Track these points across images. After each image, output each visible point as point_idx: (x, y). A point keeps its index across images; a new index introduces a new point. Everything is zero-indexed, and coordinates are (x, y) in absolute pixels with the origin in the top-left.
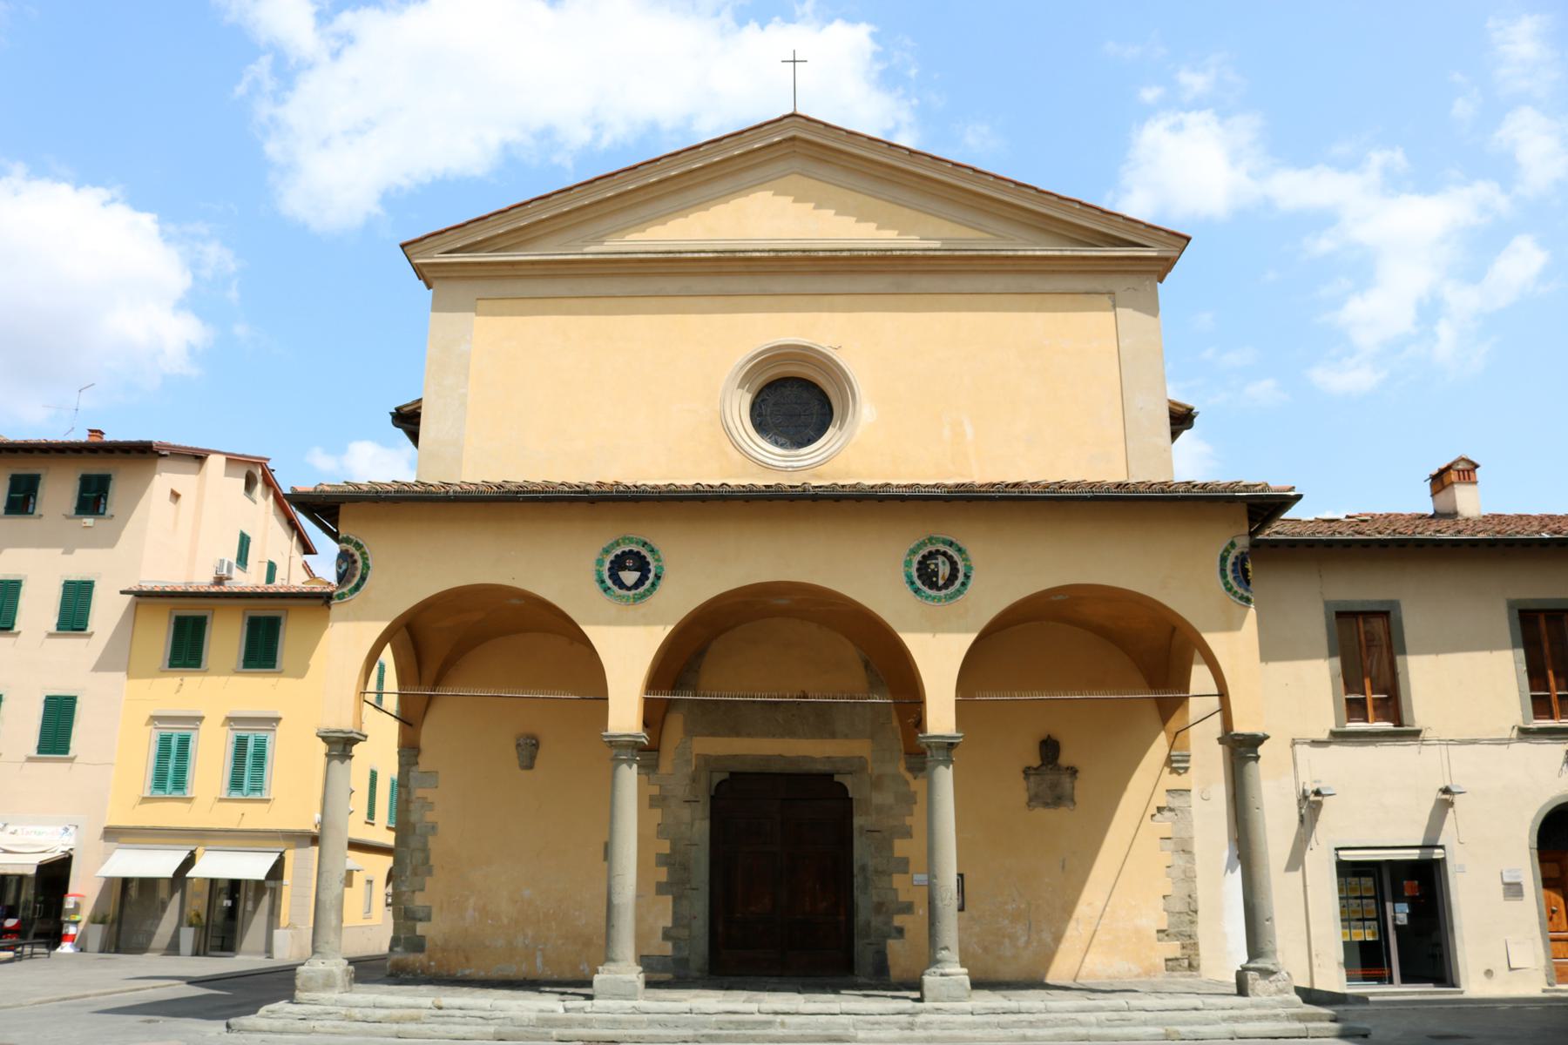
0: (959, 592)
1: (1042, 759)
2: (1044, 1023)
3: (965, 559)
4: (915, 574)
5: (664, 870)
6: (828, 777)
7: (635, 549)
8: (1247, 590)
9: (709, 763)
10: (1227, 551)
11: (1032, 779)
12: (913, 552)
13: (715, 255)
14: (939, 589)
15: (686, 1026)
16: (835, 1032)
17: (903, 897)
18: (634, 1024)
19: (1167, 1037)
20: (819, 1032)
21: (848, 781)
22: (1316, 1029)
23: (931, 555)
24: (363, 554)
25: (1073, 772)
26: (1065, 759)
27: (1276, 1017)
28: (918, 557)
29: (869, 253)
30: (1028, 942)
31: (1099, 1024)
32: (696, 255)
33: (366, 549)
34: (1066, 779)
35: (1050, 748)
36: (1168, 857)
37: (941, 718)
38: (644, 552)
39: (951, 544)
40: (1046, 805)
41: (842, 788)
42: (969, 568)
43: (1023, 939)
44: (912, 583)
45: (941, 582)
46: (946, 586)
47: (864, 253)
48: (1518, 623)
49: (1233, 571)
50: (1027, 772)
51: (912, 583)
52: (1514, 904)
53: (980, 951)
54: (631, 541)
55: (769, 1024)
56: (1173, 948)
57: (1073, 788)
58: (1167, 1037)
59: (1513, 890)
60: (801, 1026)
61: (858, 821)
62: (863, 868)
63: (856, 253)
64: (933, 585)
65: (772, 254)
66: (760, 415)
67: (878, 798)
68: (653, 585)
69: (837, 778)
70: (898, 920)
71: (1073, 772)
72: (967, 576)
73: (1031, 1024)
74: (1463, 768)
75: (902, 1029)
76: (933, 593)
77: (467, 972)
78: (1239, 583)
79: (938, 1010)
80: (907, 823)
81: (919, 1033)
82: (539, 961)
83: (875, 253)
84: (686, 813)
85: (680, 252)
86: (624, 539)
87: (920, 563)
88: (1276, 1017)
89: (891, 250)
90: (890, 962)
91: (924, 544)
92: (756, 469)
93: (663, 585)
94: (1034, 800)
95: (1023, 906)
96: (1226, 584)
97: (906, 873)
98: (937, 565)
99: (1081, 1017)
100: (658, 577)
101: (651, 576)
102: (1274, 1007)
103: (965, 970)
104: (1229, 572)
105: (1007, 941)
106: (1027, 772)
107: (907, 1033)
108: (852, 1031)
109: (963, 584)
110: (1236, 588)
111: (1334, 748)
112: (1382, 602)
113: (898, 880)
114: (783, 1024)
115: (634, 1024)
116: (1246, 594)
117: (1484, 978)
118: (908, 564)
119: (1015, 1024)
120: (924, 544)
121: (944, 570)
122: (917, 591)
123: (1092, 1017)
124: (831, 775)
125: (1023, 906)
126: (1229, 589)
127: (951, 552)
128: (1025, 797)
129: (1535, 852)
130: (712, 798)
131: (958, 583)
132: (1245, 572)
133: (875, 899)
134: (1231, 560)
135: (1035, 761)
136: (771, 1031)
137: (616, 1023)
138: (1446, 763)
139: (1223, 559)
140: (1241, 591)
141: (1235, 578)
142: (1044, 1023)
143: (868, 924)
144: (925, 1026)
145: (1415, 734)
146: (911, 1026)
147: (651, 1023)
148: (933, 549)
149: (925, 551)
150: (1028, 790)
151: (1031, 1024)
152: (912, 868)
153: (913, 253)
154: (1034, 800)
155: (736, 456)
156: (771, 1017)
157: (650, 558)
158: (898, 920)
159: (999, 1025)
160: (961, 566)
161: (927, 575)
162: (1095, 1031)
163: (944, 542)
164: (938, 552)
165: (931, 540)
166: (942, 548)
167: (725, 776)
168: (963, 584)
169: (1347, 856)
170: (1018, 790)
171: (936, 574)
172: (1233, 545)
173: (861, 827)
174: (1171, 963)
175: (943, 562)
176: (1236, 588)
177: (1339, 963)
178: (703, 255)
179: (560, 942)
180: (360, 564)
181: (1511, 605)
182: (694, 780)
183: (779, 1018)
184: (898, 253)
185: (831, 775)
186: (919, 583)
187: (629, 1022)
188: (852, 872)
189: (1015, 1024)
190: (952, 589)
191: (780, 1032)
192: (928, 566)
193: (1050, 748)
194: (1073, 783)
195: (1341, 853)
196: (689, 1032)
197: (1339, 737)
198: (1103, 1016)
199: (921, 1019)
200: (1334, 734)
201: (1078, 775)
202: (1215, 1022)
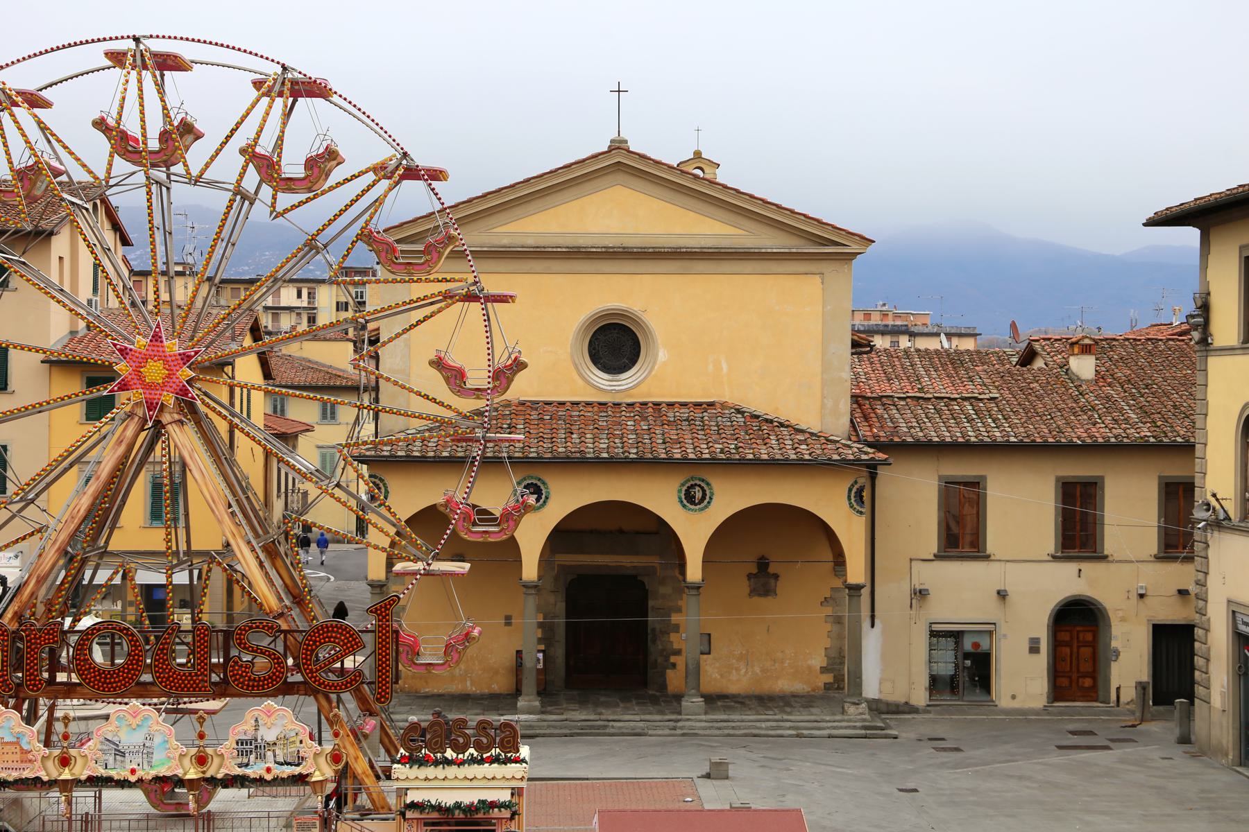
0: (706, 507)
1: (758, 569)
2: (739, 728)
3: (711, 489)
4: (683, 497)
5: (540, 630)
6: (635, 577)
7: (534, 482)
8: (861, 507)
9: (564, 569)
10: (853, 485)
11: (752, 580)
12: (683, 485)
13: (567, 250)
14: (696, 505)
15: (565, 728)
16: (638, 731)
17: (676, 646)
18: (540, 728)
19: (798, 736)
20: (630, 731)
21: (646, 580)
22: (871, 734)
23: (693, 486)
24: (384, 484)
25: (776, 577)
26: (772, 569)
27: (855, 728)
28: (685, 488)
29: (666, 250)
30: (746, 672)
31: (767, 728)
32: (555, 250)
33: (386, 481)
34: (772, 581)
35: (763, 565)
36: (829, 627)
37: (694, 571)
38: (539, 483)
39: (703, 480)
40: (760, 595)
41: (643, 583)
42: (712, 494)
43: (744, 671)
44: (682, 502)
45: (697, 501)
46: (700, 503)
47: (663, 250)
48: (1060, 491)
49: (855, 497)
50: (750, 576)
51: (682, 502)
52: (1034, 656)
53: (719, 677)
54: (532, 478)
55: (605, 727)
56: (828, 678)
57: (776, 586)
58: (798, 736)
59: (1034, 649)
60: (620, 728)
61: (651, 603)
62: (654, 630)
63: (657, 250)
64: (693, 503)
65: (603, 250)
66: (594, 349)
67: (664, 590)
68: (544, 502)
69: (639, 578)
70: (673, 659)
71: (776, 577)
72: (711, 498)
73: (733, 728)
74: (1016, 578)
75: (670, 729)
76: (692, 507)
77: (427, 690)
78: (857, 504)
79: (688, 720)
80: (679, 604)
81: (679, 732)
82: (468, 684)
83: (670, 250)
84: (552, 599)
85: (544, 247)
86: (528, 477)
87: (686, 490)
88: (855, 728)
89: (681, 248)
90: (668, 682)
91: (688, 480)
92: (593, 391)
93: (551, 503)
94: (754, 592)
95: (744, 652)
96: (850, 503)
97: (678, 632)
98: (695, 493)
99: (758, 724)
100: (547, 498)
101: (543, 497)
102: (855, 722)
103: (702, 699)
104: (852, 497)
105: (734, 671)
106: (750, 576)
107: (673, 732)
108: (646, 731)
109: (709, 503)
110: (855, 506)
111: (935, 563)
112: (975, 476)
113: (673, 637)
114: (613, 727)
115: (540, 728)
116: (860, 510)
117: (1011, 700)
118: (680, 491)
119: (726, 728)
120: (688, 480)
121: (699, 495)
122: (684, 506)
123: (763, 725)
124: (636, 576)
125: (744, 652)
126: (851, 507)
127: (703, 484)
128: (748, 590)
129: (1050, 628)
130: (567, 589)
131: (706, 502)
132: (861, 497)
133: (660, 647)
134: (854, 490)
135: (755, 571)
136: (607, 731)
137: (531, 727)
138: (1003, 574)
139: (850, 490)
140: (858, 508)
141: (855, 501)
142: (739, 728)
143: (656, 661)
144: (681, 728)
145: (988, 556)
146: (674, 728)
147: (549, 727)
148: (693, 483)
149: (688, 484)
150: (750, 586)
151: (733, 728)
152: (681, 629)
153: (694, 250)
154: (754, 592)
155: (580, 382)
156: (606, 723)
157: (542, 487)
158: (673, 659)
159: (719, 729)
160: (708, 492)
161: (690, 498)
162: (763, 732)
163: (700, 480)
164: (696, 485)
165: (692, 478)
166: (698, 482)
167: (575, 576)
168: (709, 503)
169: (936, 627)
170: (744, 587)
171: (695, 497)
172: (856, 482)
173: (653, 607)
174: (828, 687)
175: (699, 491)
176: (855, 506)
177: (926, 689)
178: (559, 250)
179: (480, 672)
180: (383, 490)
181: (1058, 479)
182: (556, 579)
183: (611, 723)
184: (684, 250)
185: (636, 576)
186: (685, 502)
187: (538, 726)
188: (647, 632)
189: (726, 728)
190: (702, 505)
191: (612, 731)
192: (690, 493)
193: (763, 565)
194: (776, 583)
195: (933, 626)
196: (568, 731)
197: (938, 557)
198: (769, 724)
199: (680, 724)
200: (935, 556)
201: (780, 578)
202: (824, 729)
